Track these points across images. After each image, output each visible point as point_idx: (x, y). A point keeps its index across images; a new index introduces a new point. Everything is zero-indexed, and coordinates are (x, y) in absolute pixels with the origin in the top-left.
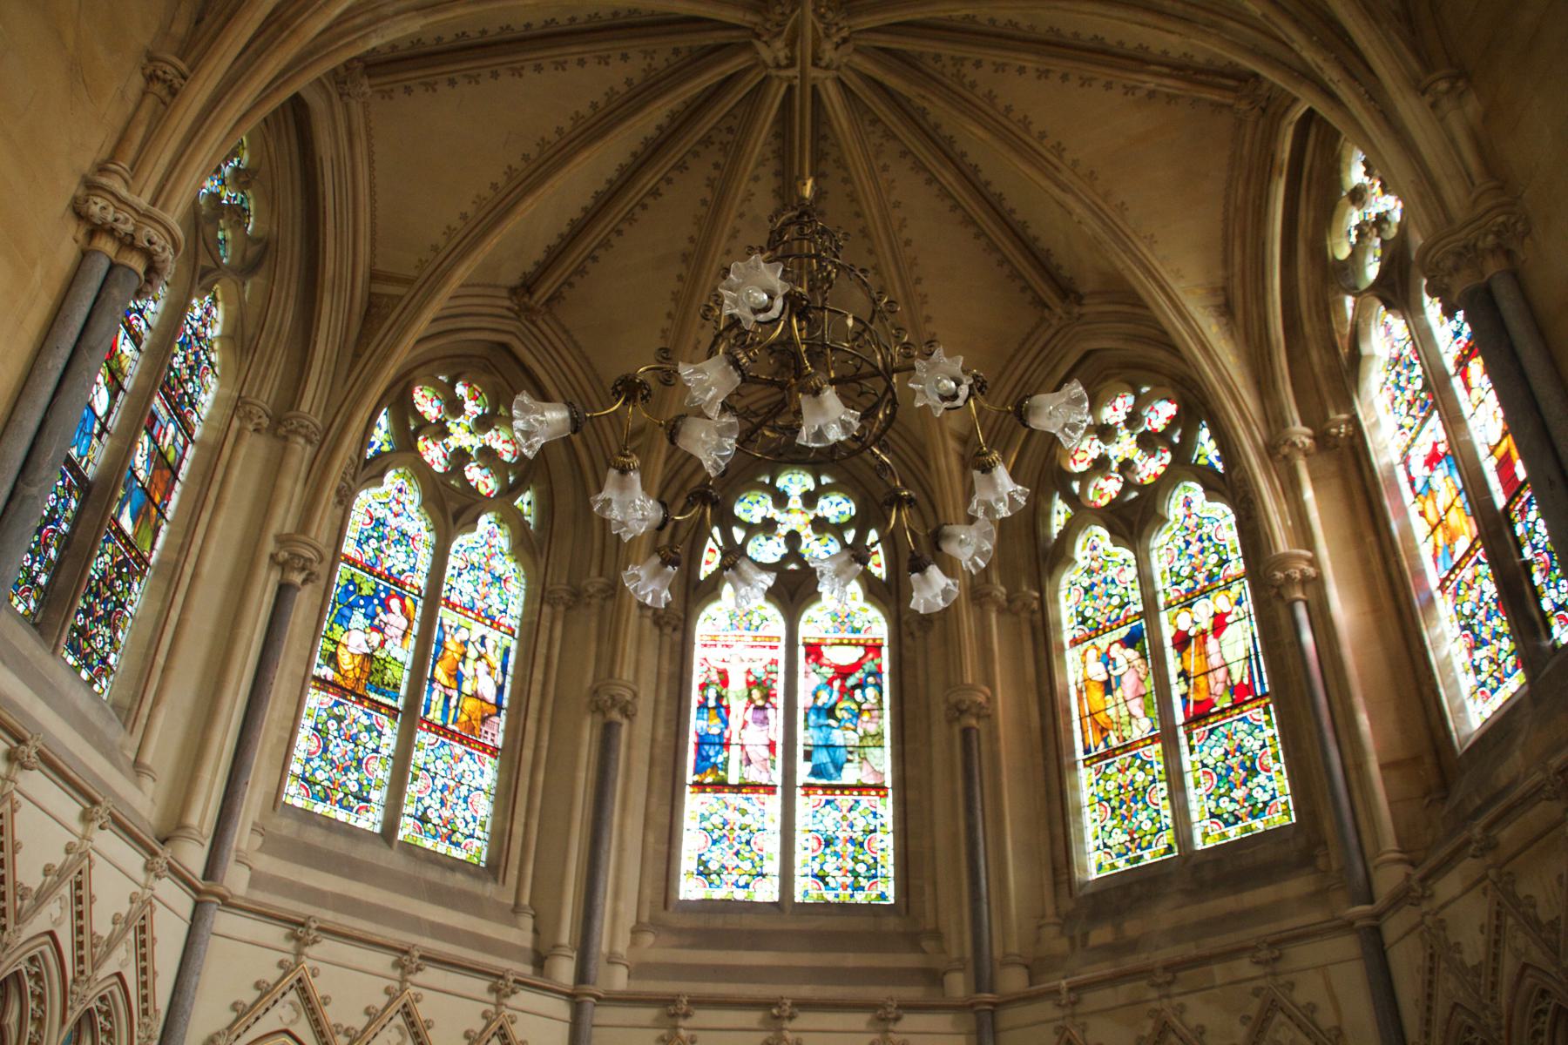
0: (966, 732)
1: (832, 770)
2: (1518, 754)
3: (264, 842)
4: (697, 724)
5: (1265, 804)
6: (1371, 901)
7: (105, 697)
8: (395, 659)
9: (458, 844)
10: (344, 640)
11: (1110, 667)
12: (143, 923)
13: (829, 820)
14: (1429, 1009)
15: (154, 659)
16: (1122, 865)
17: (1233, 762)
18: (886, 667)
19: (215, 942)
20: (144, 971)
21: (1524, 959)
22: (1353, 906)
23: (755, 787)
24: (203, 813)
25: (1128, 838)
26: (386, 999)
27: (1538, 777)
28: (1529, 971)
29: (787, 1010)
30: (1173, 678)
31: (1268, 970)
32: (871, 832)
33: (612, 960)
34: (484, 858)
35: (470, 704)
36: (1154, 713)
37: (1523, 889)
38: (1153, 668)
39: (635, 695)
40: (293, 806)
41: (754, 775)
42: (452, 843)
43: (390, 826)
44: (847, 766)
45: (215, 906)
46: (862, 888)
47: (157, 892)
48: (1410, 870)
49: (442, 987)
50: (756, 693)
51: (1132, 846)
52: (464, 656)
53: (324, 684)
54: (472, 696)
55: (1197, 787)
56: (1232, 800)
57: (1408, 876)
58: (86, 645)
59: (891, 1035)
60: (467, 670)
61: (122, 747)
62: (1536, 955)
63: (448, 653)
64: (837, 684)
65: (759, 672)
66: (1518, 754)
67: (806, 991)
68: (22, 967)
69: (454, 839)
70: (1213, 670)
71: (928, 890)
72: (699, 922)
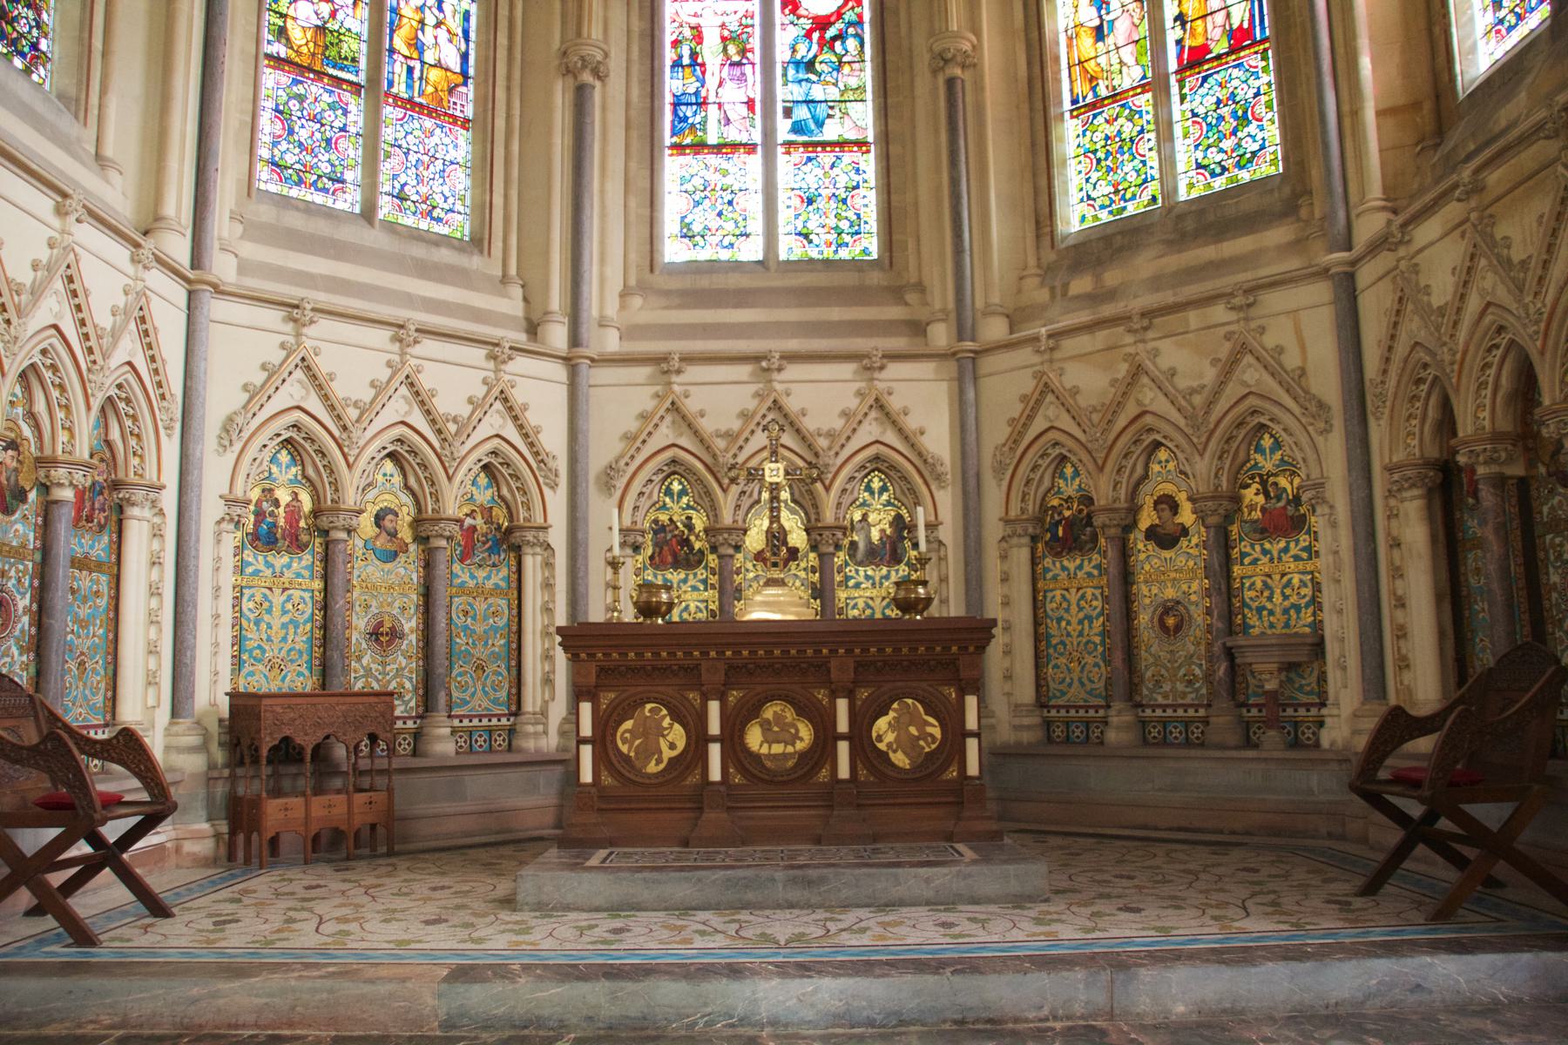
0: (951, 83)
1: (812, 126)
2: (1523, 95)
3: (245, 230)
4: (673, 84)
5: (1254, 154)
6: (1349, 249)
7: (47, 86)
8: (349, 30)
9: (439, 220)
10: (291, 12)
11: (1103, 12)
12: (141, 313)
13: (812, 176)
14: (1390, 348)
15: (90, 46)
16: (1105, 217)
17: (1225, 111)
18: (867, 17)
21: (1488, 298)
22: (1331, 253)
23: (735, 146)
24: (178, 201)
25: (1112, 190)
26: (389, 372)
27: (1542, 114)
28: (1491, 310)
29: (776, 363)
30: (1169, 23)
31: (1242, 315)
32: (854, 188)
33: (602, 324)
34: (467, 232)
35: (434, 75)
36: (1146, 60)
37: (1501, 231)
38: (1149, 12)
39: (606, 55)
40: (267, 191)
41: (734, 134)
42: (433, 219)
43: (368, 212)
44: (828, 121)
46: (847, 245)
47: (148, 283)
48: (1391, 216)
49: (440, 357)
50: (732, 49)
51: (1117, 199)
52: (422, 22)
53: (278, 62)
54: (435, 66)
55: (1185, 137)
56: (1221, 151)
57: (1389, 222)
58: (10, 29)
59: (876, 382)
60: (427, 38)
61: (79, 140)
62: (1503, 295)
63: (405, 21)
64: (816, 35)
65: (734, 26)
66: (1523, 95)
67: (793, 345)
68: (35, 359)
69: (435, 214)
70: (1211, 13)
71: (911, 245)
72: (687, 283)
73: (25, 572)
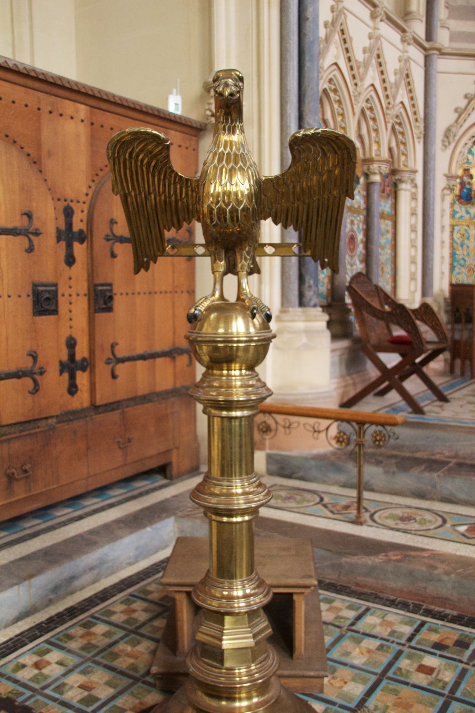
19: (440, 76)
20: (412, 98)
45: (436, 56)
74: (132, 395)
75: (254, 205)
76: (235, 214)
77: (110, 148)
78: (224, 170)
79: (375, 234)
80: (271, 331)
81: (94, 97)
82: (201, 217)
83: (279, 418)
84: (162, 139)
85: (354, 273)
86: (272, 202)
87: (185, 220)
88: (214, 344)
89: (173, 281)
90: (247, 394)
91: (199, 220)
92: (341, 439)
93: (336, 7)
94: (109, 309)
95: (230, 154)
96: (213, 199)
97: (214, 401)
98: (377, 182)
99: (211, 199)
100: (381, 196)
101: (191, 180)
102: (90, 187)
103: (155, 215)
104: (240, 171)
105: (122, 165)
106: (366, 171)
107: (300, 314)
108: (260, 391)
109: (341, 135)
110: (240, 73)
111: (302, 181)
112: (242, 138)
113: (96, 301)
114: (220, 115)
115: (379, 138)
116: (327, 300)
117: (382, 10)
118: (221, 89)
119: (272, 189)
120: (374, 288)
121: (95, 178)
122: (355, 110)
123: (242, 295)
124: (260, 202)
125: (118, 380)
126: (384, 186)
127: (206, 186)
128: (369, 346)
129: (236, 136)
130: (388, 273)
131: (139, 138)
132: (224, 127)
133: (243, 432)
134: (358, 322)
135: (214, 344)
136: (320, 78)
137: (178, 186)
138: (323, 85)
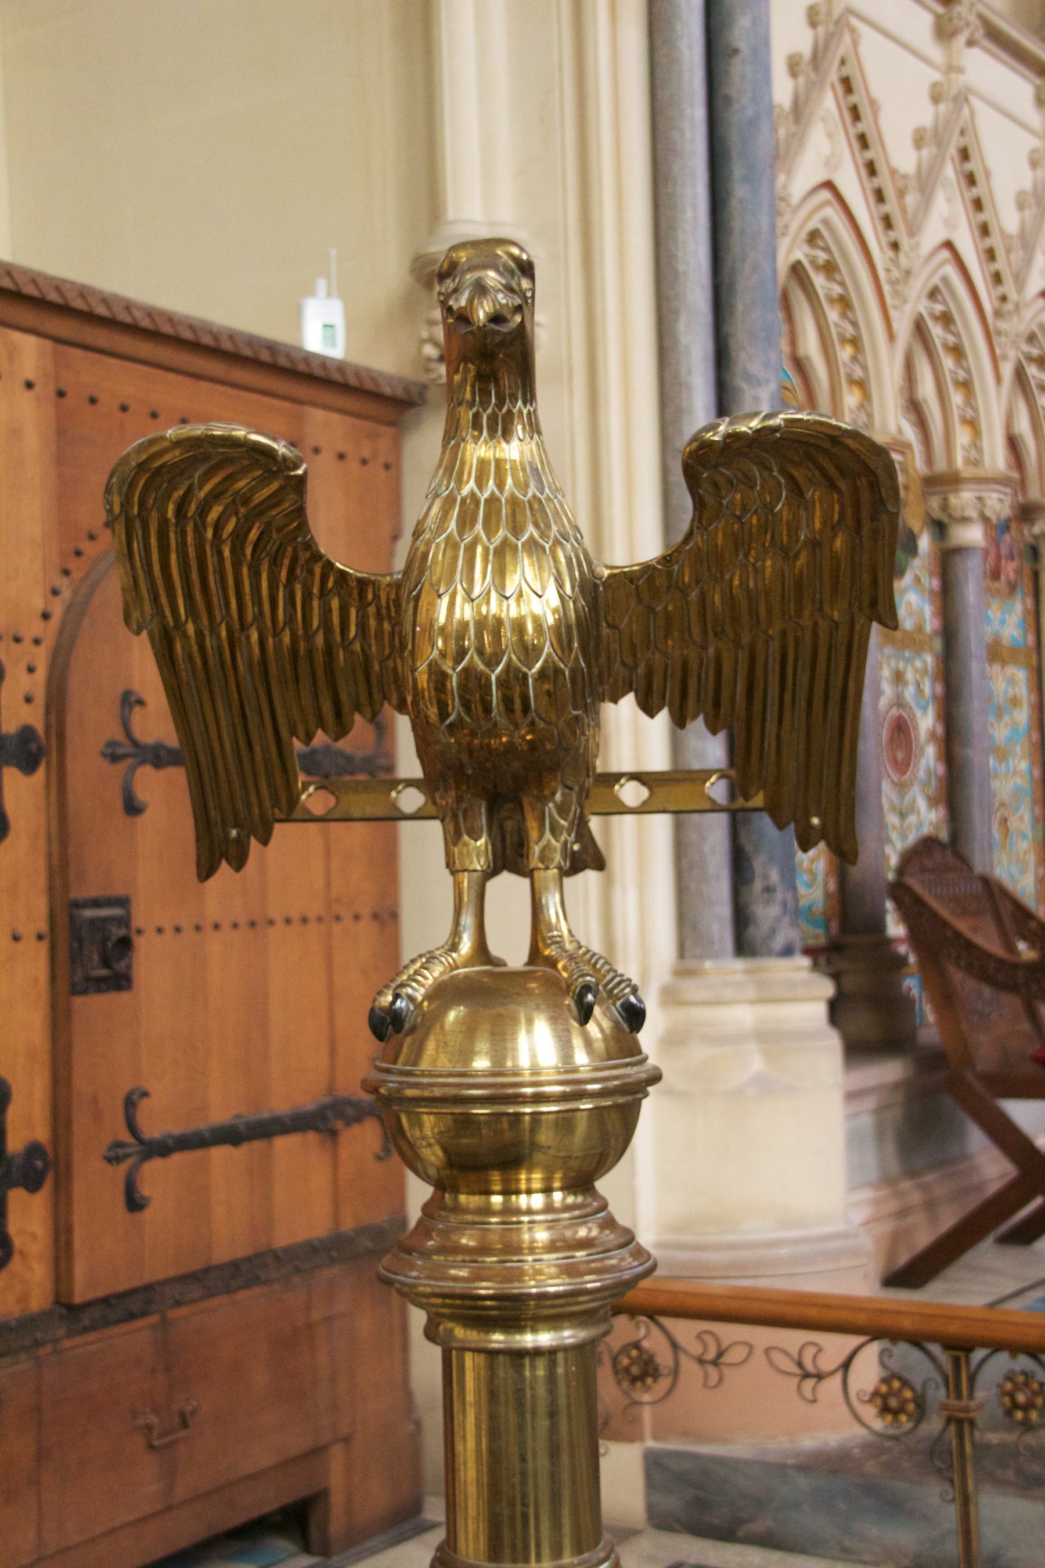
73: (925, 671)
74: (194, 1264)
75: (577, 659)
76: (517, 690)
77: (115, 489)
78: (479, 550)
79: (974, 709)
80: (646, 1059)
81: (64, 310)
82: (409, 699)
83: (684, 1330)
84: (280, 458)
85: (912, 838)
86: (633, 647)
87: (358, 708)
88: (458, 1110)
89: (328, 885)
90: (570, 1270)
91: (401, 708)
92: (893, 1403)
93: (823, 9)
94: (121, 982)
95: (498, 500)
96: (445, 642)
97: (463, 1297)
98: (975, 549)
99: (440, 643)
100: (988, 590)
101: (374, 583)
102: (55, 592)
103: (262, 693)
104: (530, 555)
105: (153, 541)
106: (937, 514)
107: (739, 977)
108: (614, 1262)
109: (846, 431)
110: (522, 249)
111: (727, 577)
112: (534, 448)
113: (75, 957)
114: (464, 380)
115: (976, 410)
116: (827, 928)
117: (970, 10)
118: (463, 303)
119: (633, 603)
120: (978, 887)
121: (73, 564)
122: (895, 326)
123: (548, 946)
124: (597, 646)
125: (147, 1214)
126: (999, 557)
127: (423, 603)
128: (969, 1077)
129: (515, 443)
130: (1024, 836)
131: (206, 458)
132: (477, 416)
133: (562, 1401)
134: (932, 1000)
135: (458, 1110)
136: (778, 231)
137: (335, 603)
138: (790, 251)
